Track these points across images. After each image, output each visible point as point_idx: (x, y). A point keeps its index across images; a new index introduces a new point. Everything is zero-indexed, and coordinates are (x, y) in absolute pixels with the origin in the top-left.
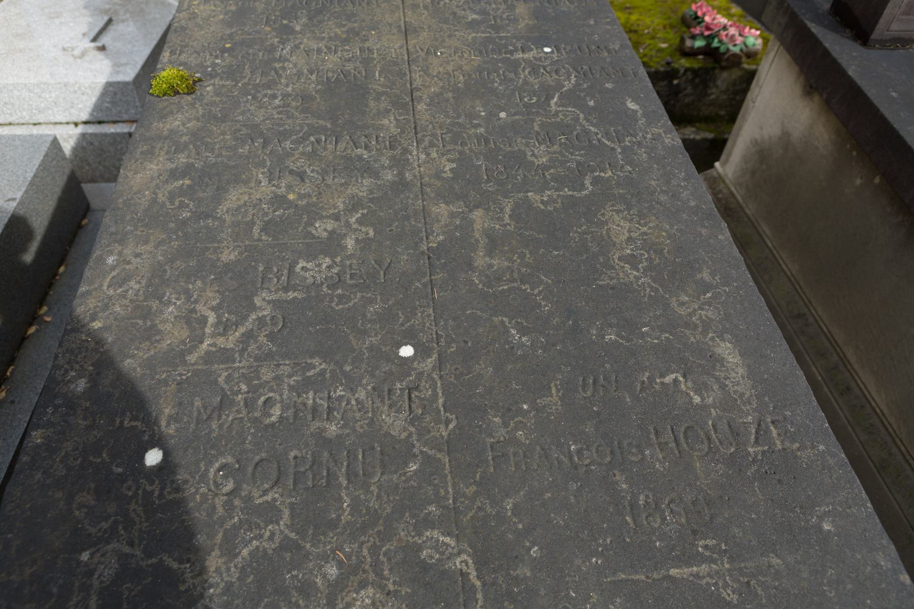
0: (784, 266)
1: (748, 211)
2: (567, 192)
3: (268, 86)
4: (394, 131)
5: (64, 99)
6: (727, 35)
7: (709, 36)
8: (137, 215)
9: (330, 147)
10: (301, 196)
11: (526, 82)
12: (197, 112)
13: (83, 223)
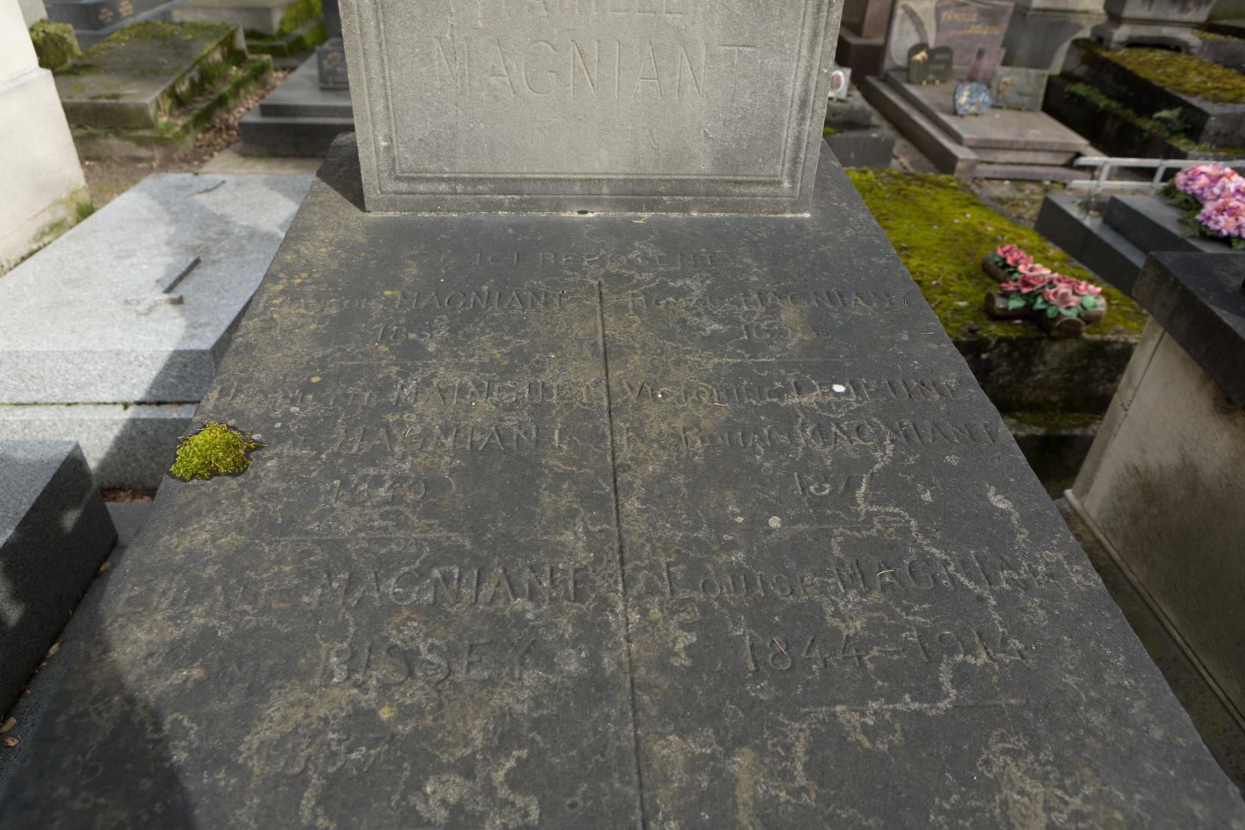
0: (1210, 681)
1: (1131, 576)
2: (909, 703)
3: (370, 459)
4: (584, 557)
5: (113, 372)
6: (1055, 294)
7: (1028, 294)
8: (84, 755)
9: (467, 592)
10: (405, 712)
11: (809, 454)
12: (243, 514)
13: (102, 569)
